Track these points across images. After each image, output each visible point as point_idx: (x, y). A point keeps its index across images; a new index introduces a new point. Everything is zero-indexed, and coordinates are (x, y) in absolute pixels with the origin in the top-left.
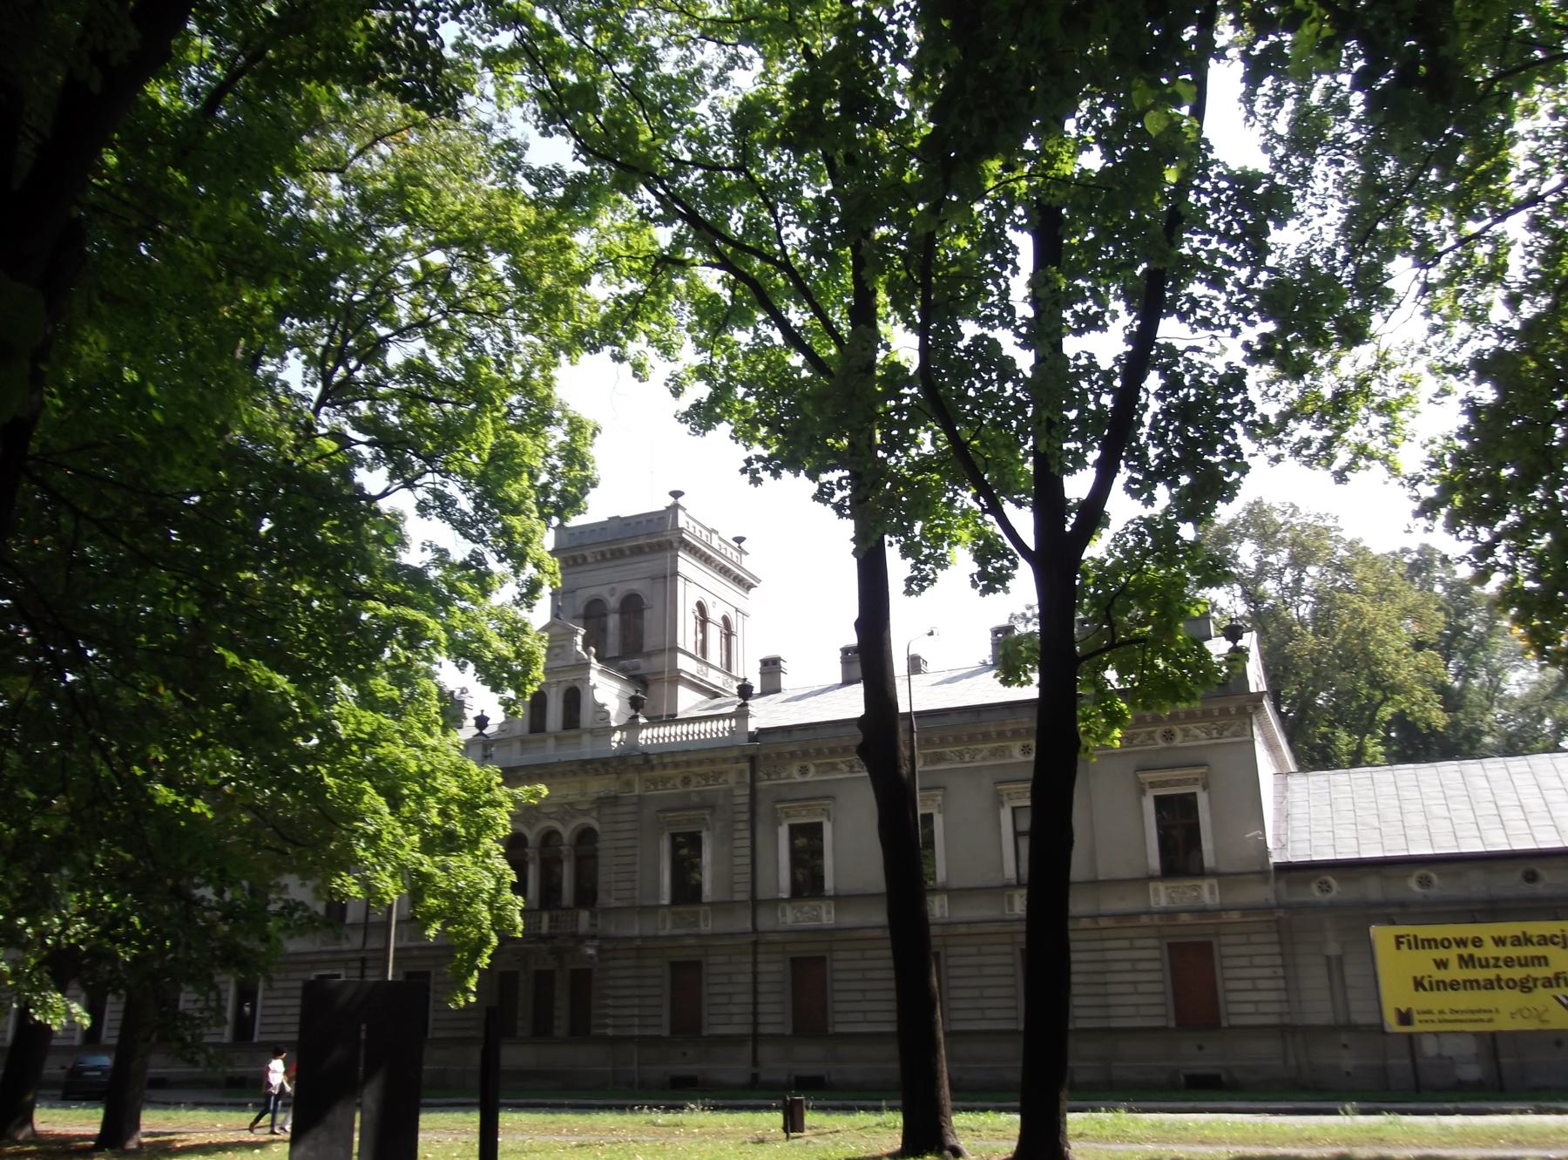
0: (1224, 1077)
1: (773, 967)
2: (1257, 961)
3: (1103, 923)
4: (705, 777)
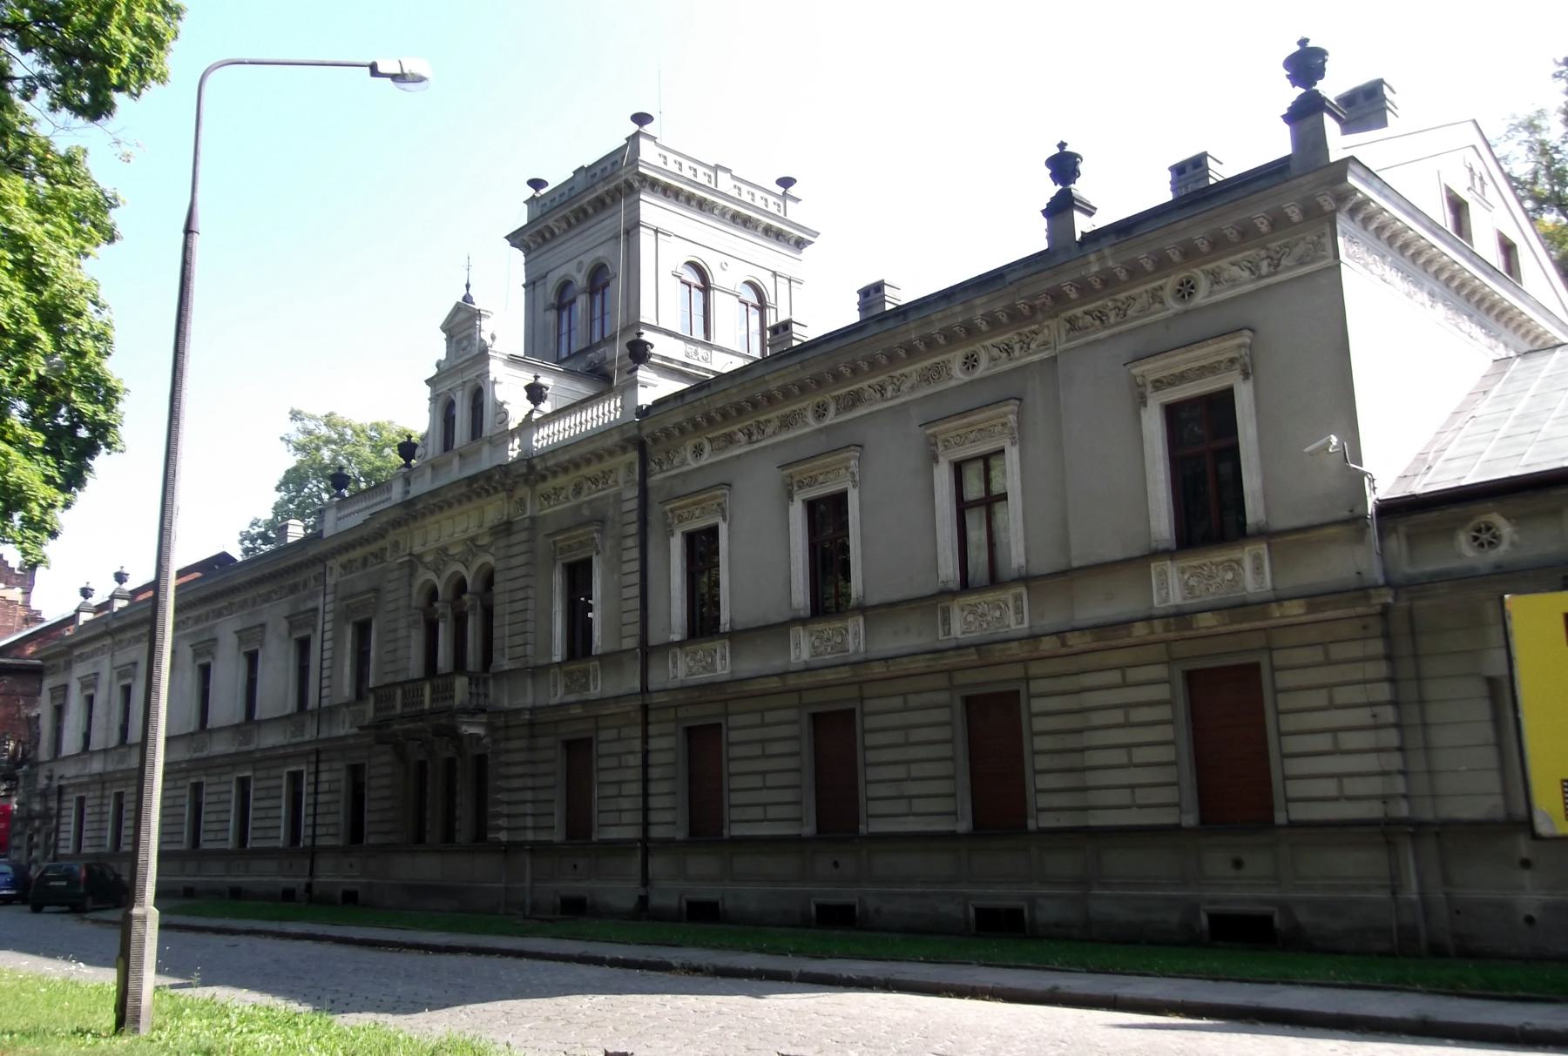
0: (1277, 921)
2: (1342, 696)
3: (1076, 642)
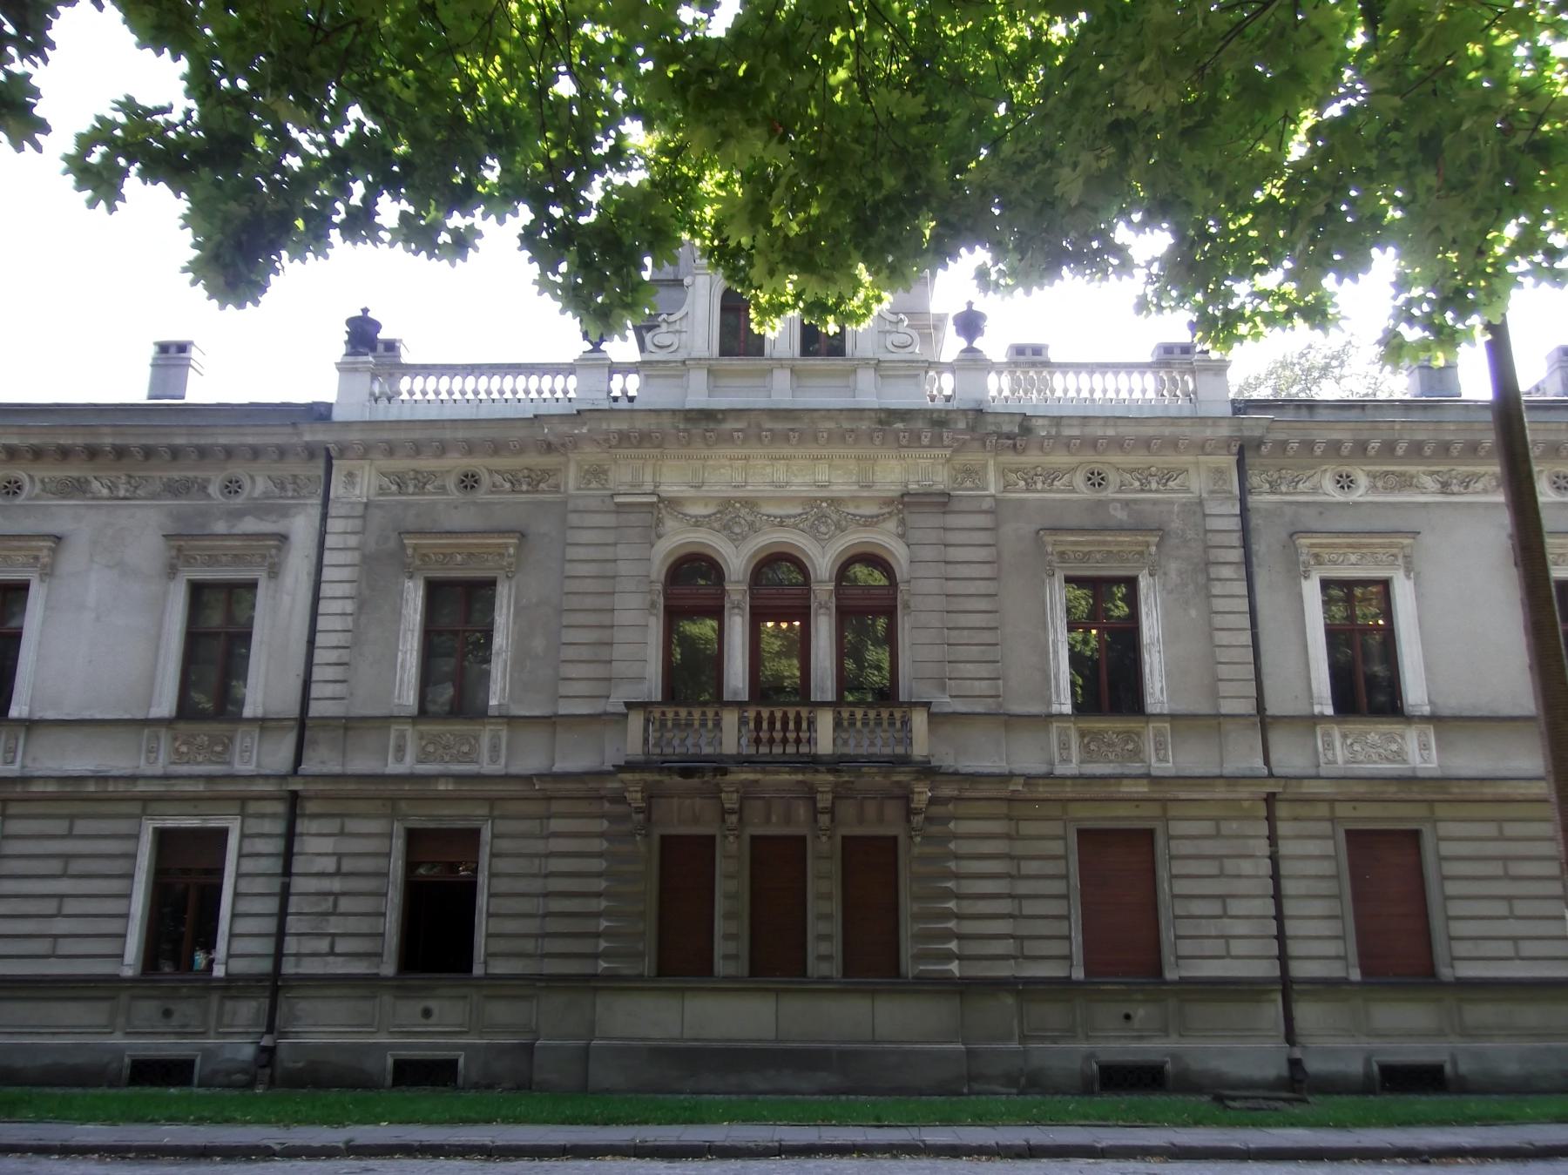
1: (1312, 847)
4: (1144, 475)
